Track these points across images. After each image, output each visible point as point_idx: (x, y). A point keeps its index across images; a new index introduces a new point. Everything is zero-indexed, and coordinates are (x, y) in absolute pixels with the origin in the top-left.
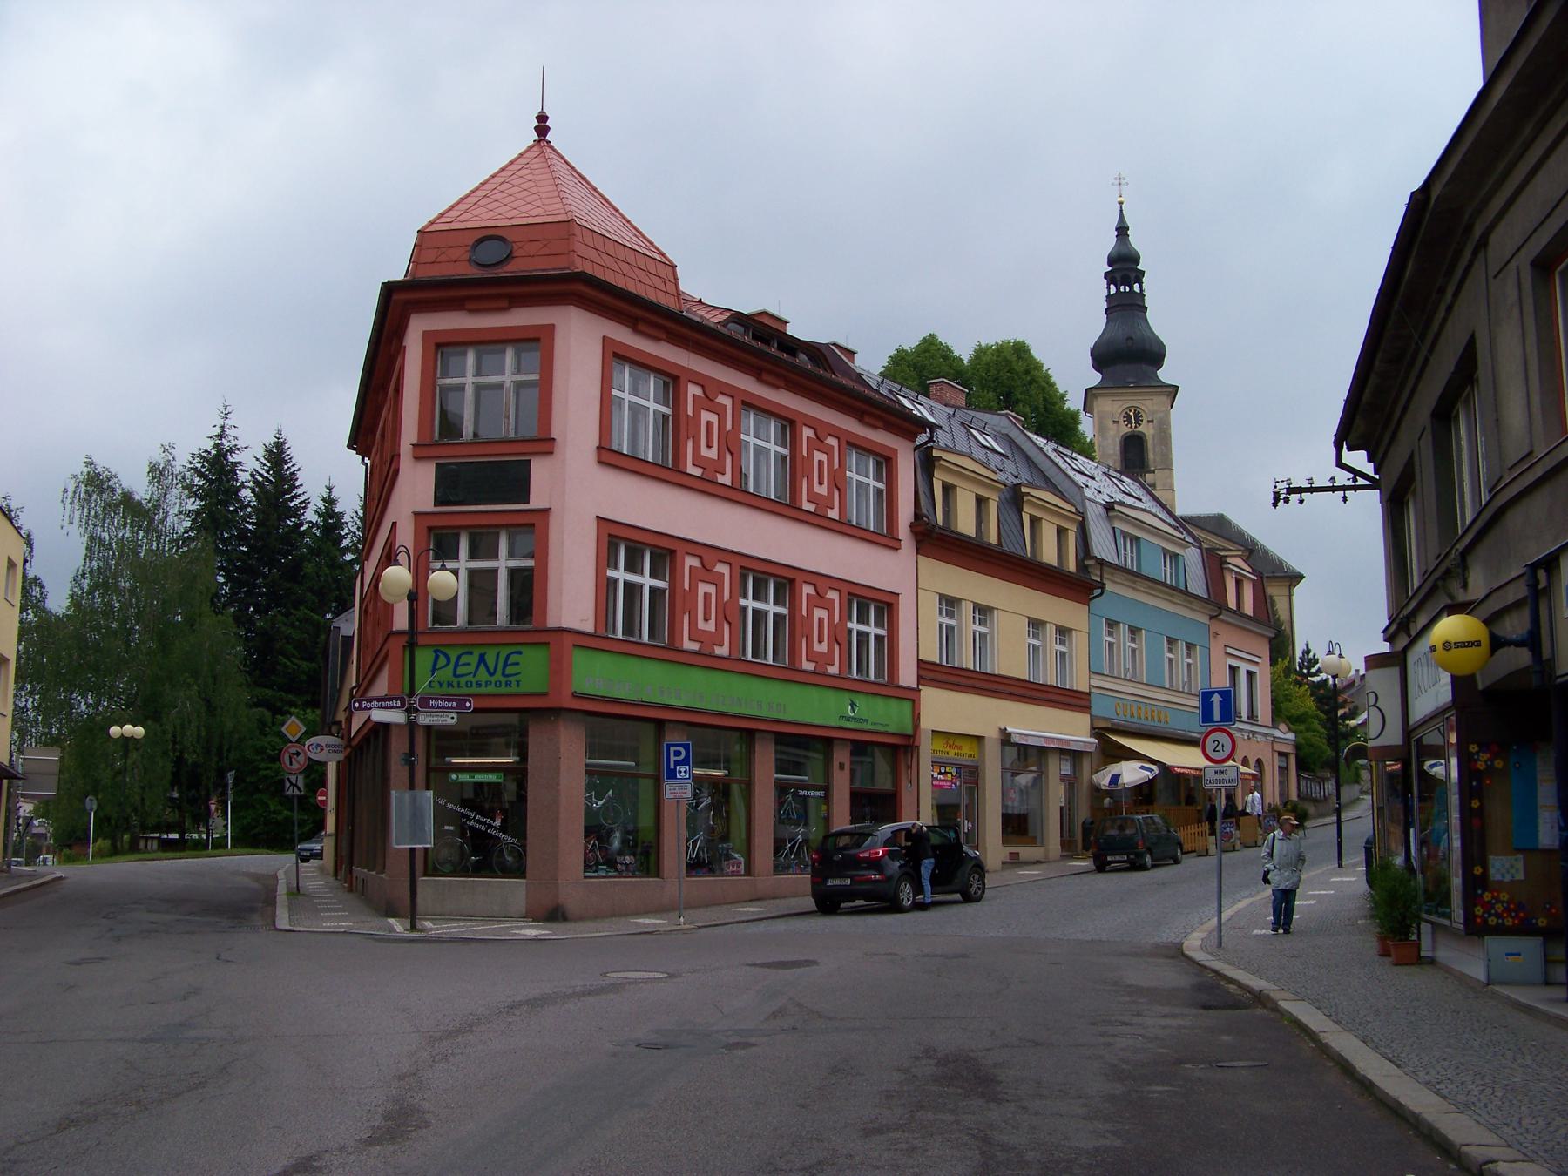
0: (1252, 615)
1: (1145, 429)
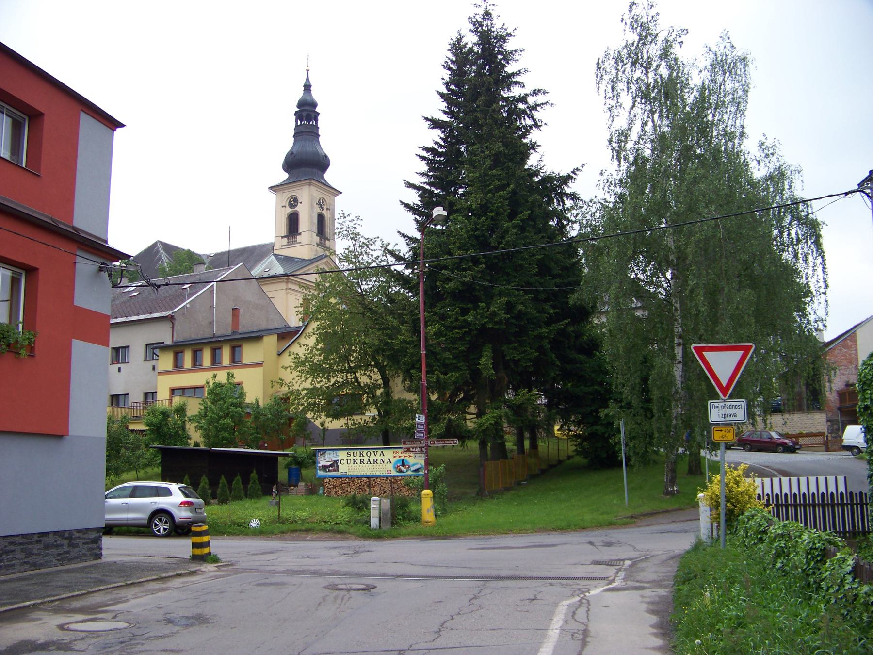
0: (704, 353)
1: (324, 212)
